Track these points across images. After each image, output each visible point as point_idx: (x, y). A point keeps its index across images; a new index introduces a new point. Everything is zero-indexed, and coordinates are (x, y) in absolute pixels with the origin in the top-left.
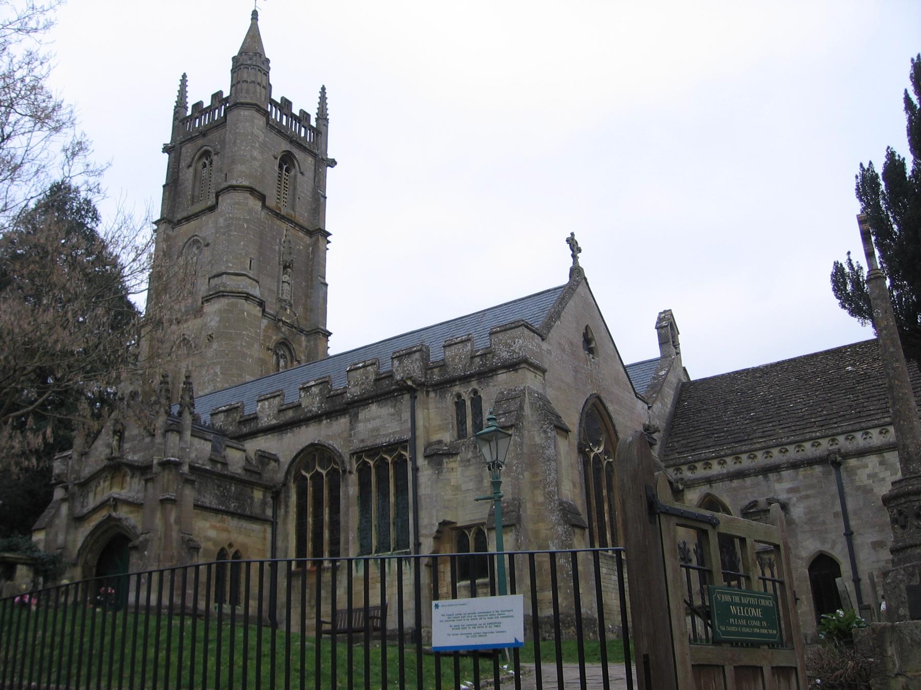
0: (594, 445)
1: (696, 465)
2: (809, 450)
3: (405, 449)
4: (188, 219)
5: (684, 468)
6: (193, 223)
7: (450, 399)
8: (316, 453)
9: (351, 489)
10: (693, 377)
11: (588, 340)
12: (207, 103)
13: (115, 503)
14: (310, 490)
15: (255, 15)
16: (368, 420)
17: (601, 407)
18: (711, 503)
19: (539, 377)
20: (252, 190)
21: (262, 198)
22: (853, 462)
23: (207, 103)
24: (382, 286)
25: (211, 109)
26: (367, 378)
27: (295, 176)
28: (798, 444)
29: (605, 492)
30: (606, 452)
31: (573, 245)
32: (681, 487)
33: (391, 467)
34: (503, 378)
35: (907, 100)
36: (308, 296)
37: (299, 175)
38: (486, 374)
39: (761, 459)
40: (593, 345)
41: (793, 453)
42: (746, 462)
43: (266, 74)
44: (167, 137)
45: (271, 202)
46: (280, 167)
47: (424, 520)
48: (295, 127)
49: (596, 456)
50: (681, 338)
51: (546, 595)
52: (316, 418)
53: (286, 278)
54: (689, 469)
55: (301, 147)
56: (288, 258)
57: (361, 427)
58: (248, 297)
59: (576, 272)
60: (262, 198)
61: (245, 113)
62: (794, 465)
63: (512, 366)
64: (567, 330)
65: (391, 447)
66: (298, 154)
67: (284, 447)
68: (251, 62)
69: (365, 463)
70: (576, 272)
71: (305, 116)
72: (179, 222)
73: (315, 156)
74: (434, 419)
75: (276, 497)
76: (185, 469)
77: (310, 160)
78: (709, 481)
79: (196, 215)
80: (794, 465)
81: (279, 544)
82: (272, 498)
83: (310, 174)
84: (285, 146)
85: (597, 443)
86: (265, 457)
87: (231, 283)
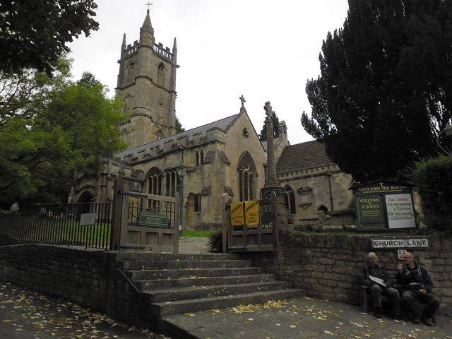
2: (320, 171)
4: (126, 87)
6: (128, 89)
7: (194, 153)
8: (155, 170)
9: (164, 182)
10: (291, 144)
12: (132, 45)
13: (88, 187)
14: (153, 182)
15: (148, 11)
18: (288, 188)
19: (223, 146)
20: (147, 78)
21: (151, 80)
22: (335, 175)
23: (132, 45)
24: (194, 111)
25: (134, 47)
28: (317, 168)
31: (242, 99)
34: (210, 146)
35: (320, 56)
36: (169, 115)
38: (205, 145)
39: (305, 174)
41: (315, 172)
42: (300, 174)
43: (153, 34)
44: (119, 57)
45: (155, 81)
46: (159, 68)
47: (184, 193)
48: (164, 53)
50: (288, 131)
51: (101, 216)
52: (155, 159)
53: (161, 108)
55: (167, 61)
56: (161, 101)
57: (167, 162)
58: (145, 116)
59: (243, 109)
60: (151, 80)
61: (144, 49)
62: (315, 176)
63: (213, 142)
64: (237, 128)
66: (165, 63)
67: (145, 168)
68: (147, 29)
70: (243, 109)
71: (168, 49)
72: (123, 89)
73: (172, 64)
74: (189, 159)
75: (142, 185)
76: (109, 176)
78: (288, 180)
79: (129, 86)
80: (315, 176)
83: (170, 70)
84: (161, 61)
85: (247, 168)
86: (139, 172)
87: (139, 110)
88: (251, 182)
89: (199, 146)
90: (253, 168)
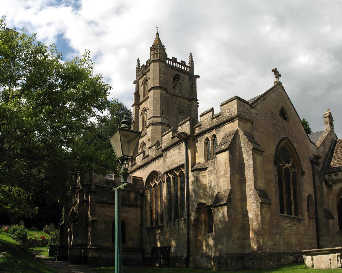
0: (286, 163)
1: (338, 173)
3: (183, 168)
5: (333, 175)
6: (144, 103)
11: (283, 114)
16: (170, 157)
17: (290, 145)
26: (169, 138)
27: (181, 82)
29: (291, 186)
30: (293, 166)
32: (331, 183)
33: (178, 178)
37: (182, 82)
40: (286, 116)
46: (174, 79)
49: (286, 169)
54: (335, 175)
65: (178, 168)
69: (169, 177)
70: (278, 86)
71: (183, 63)
77: (187, 76)
81: (144, 216)
82: (140, 196)
84: (177, 73)
85: (288, 162)
88: (295, 184)
89: (210, 130)
90: (297, 164)
